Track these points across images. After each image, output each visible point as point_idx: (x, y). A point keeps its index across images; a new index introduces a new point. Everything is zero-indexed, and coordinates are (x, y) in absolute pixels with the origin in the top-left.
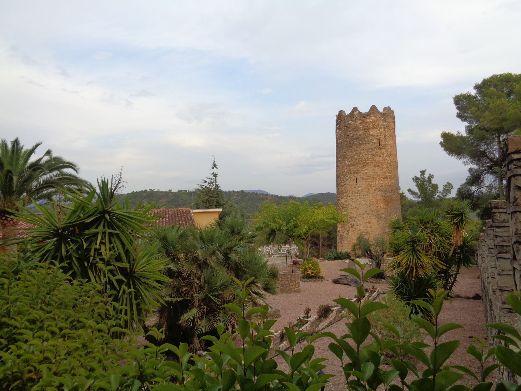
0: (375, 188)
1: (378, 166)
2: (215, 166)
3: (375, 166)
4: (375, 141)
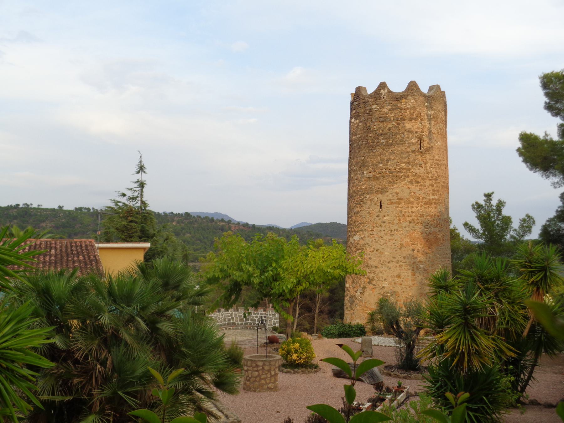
0: (410, 219)
2: (141, 168)
4: (413, 140)
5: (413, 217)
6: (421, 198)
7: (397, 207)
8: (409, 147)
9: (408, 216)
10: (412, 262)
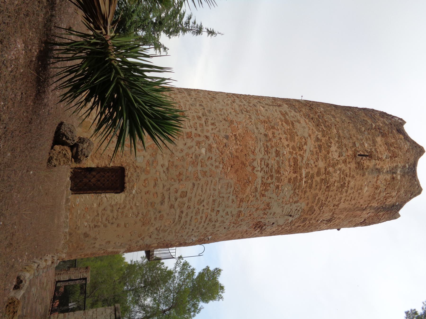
0: (271, 136)
1: (320, 147)
2: (211, 33)
3: (318, 139)
4: (366, 145)
5: (274, 140)
6: (301, 153)
7: (282, 121)
8: (357, 139)
9: (273, 133)
10: (208, 134)
